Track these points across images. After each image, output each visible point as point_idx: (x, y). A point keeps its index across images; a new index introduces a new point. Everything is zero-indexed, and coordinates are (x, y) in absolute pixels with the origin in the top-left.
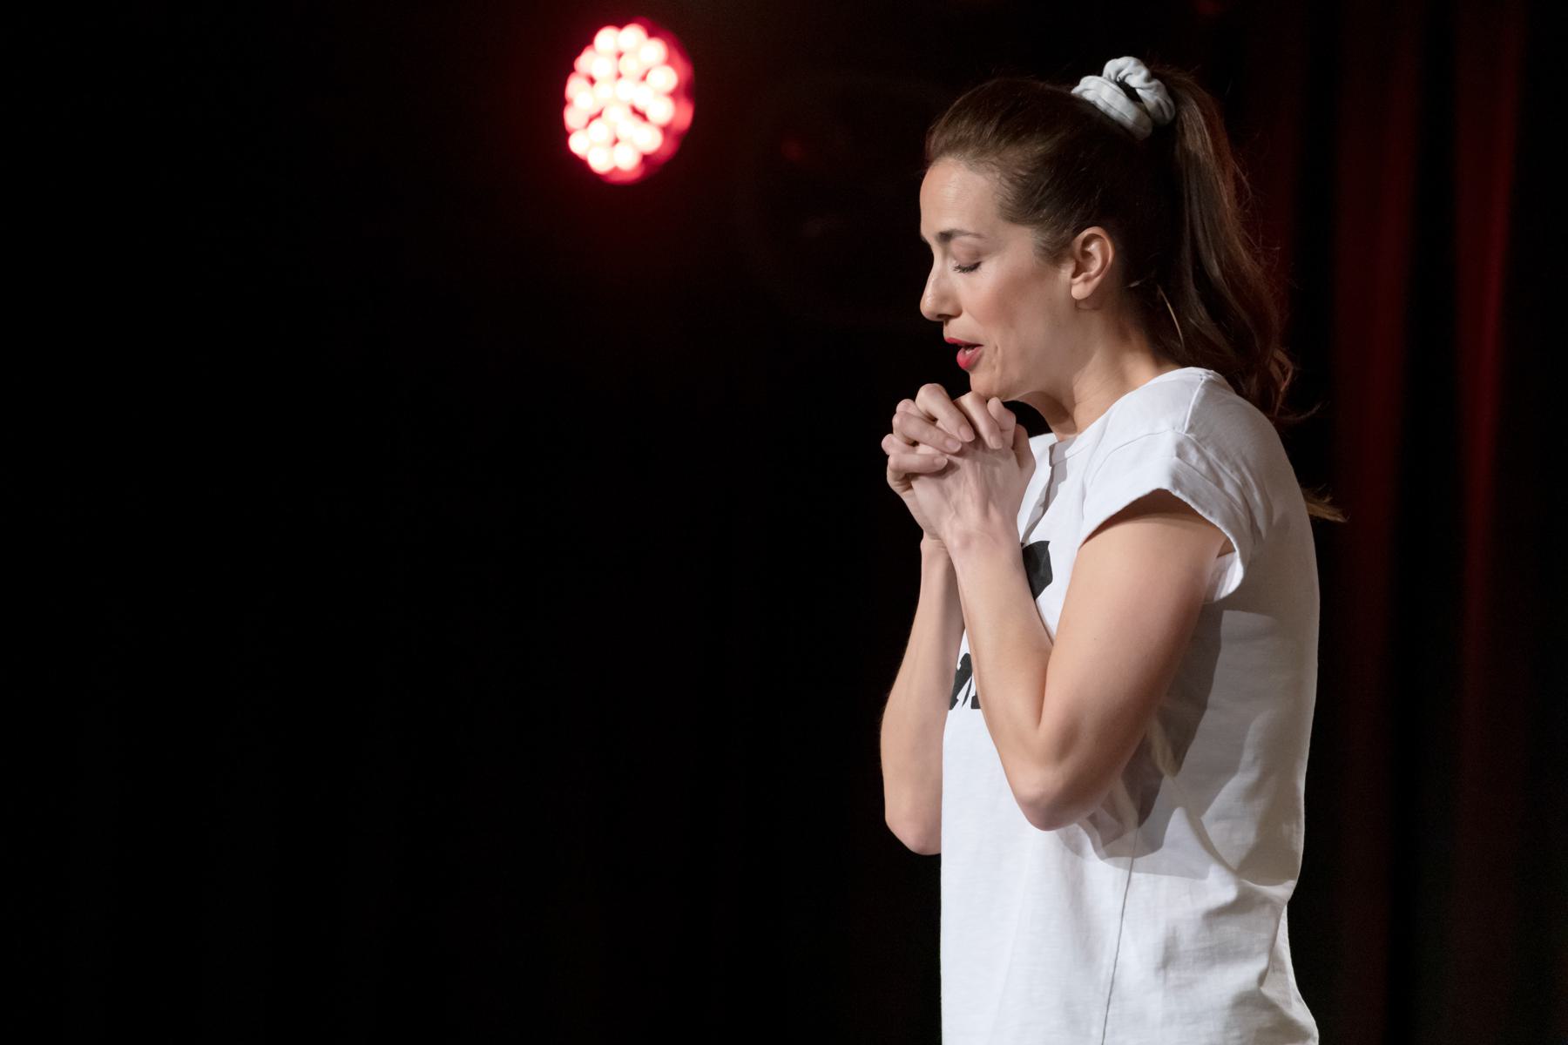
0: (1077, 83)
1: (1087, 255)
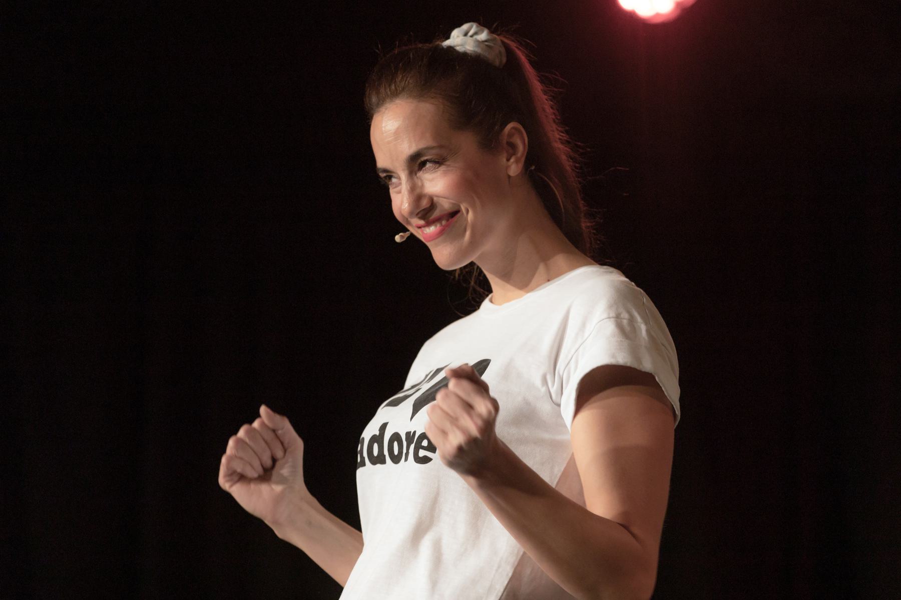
0: (448, 38)
1: (513, 146)
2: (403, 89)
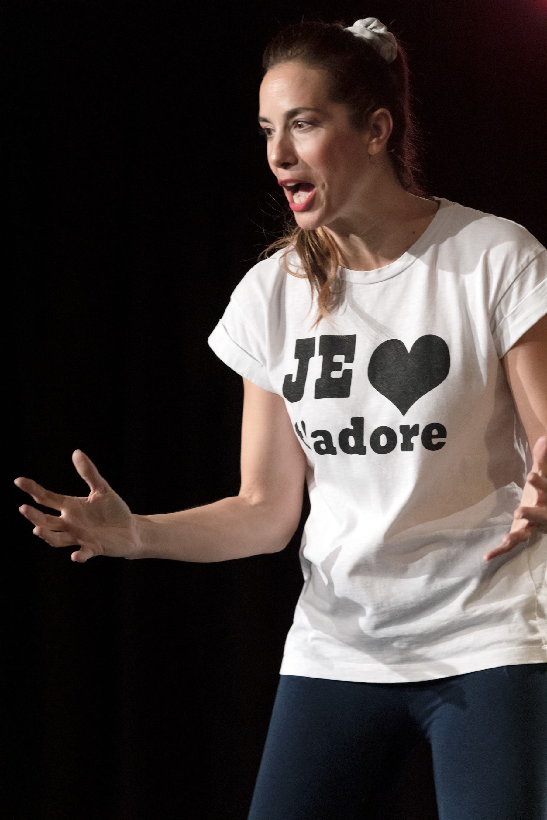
0: (351, 25)
1: (377, 128)
2: (297, 55)
